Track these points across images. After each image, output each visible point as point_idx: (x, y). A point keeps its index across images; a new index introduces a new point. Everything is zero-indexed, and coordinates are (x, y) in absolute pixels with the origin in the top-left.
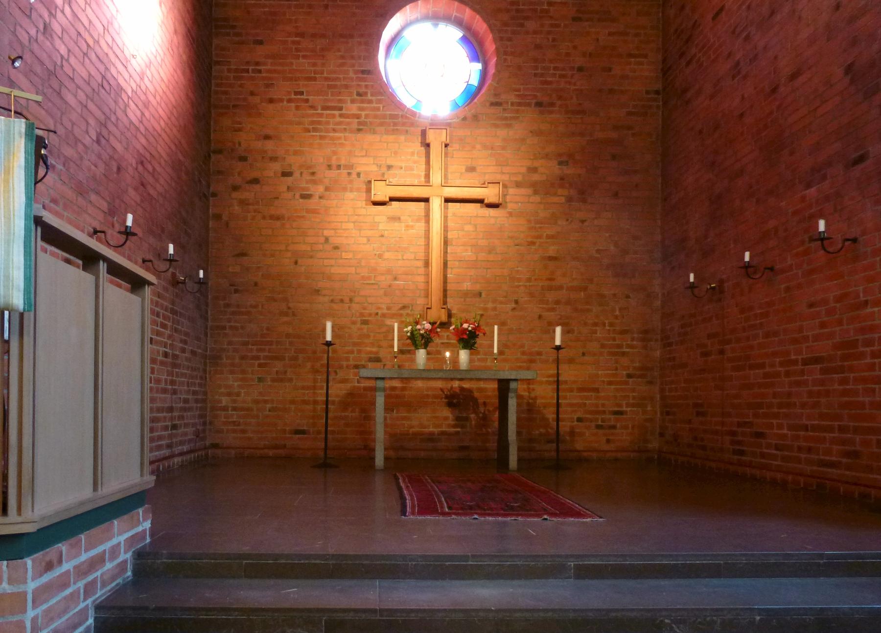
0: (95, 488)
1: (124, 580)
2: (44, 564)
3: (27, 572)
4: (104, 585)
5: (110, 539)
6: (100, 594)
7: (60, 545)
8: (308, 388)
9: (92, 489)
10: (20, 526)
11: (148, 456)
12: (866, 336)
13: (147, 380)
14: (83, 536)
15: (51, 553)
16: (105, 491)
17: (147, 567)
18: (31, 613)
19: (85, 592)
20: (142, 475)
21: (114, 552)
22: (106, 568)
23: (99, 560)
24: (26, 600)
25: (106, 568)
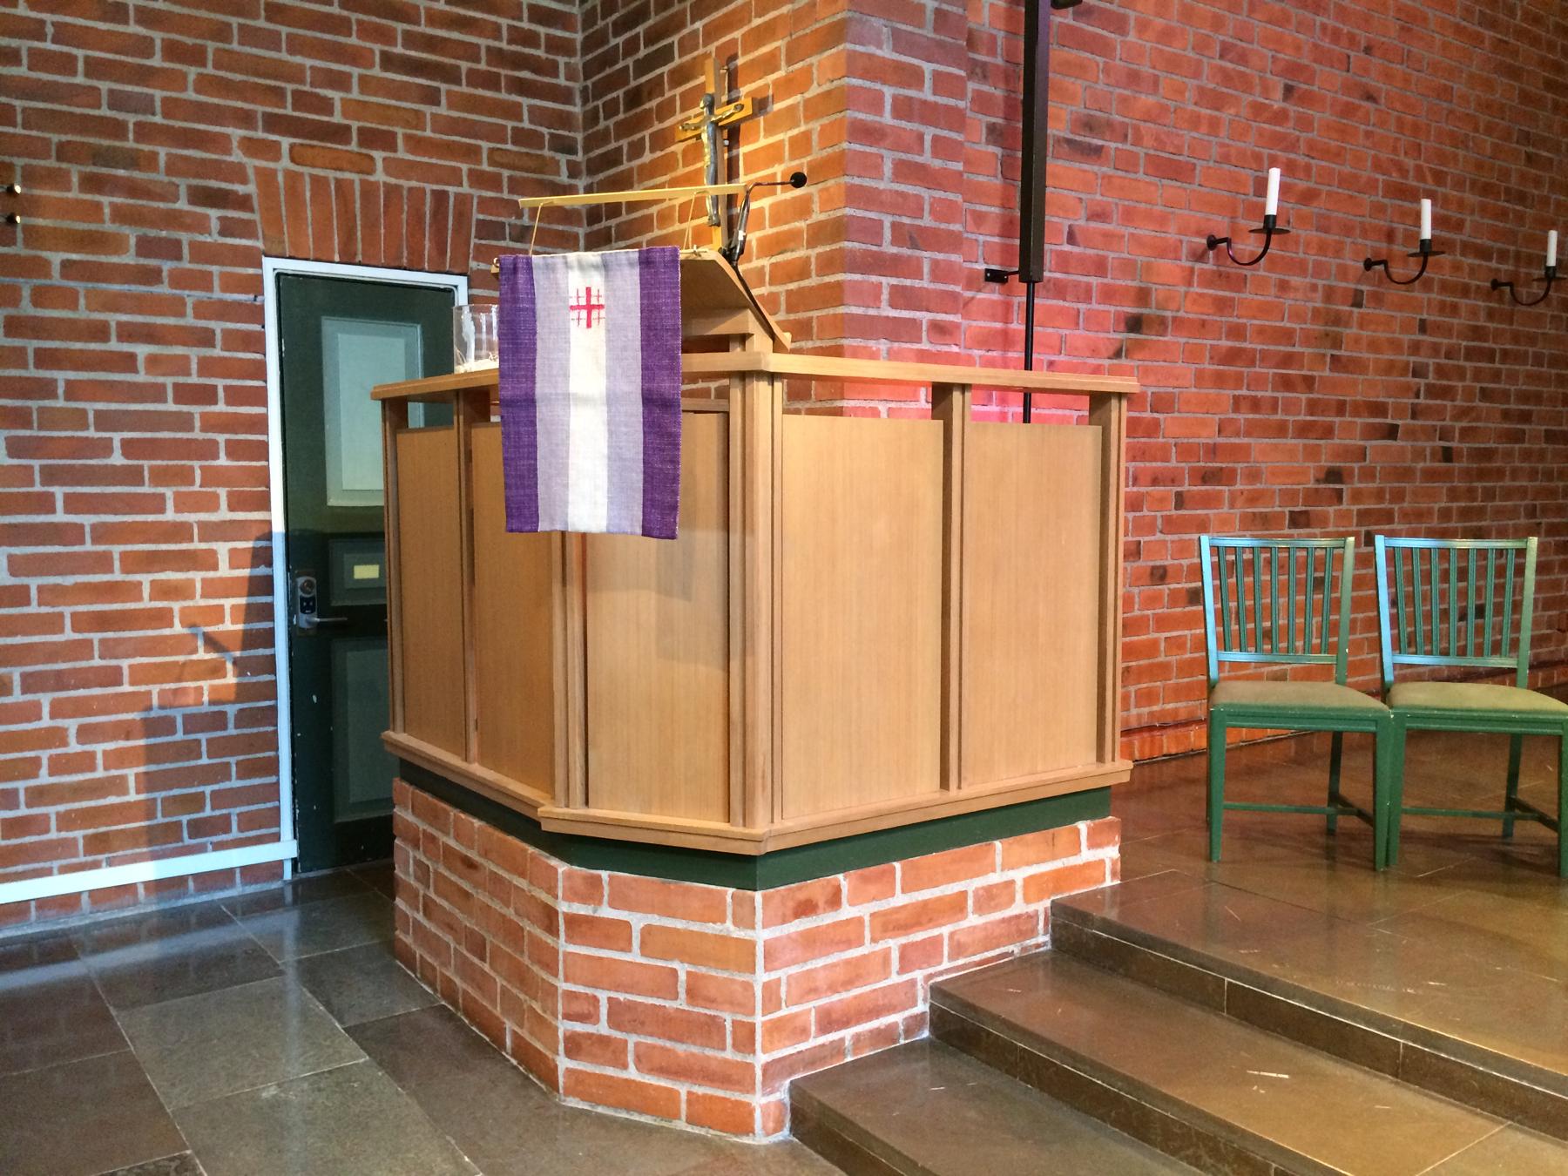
0: (944, 783)
1: (1024, 949)
2: (791, 904)
3: (754, 913)
4: (958, 950)
5: (985, 873)
6: (946, 967)
7: (841, 876)
8: (588, 300)
9: (1093, 756)
10: (738, 843)
11: (1116, 718)
12: (1155, 708)
13: (1118, 587)
14: (998, 844)
15: (815, 888)
16: (966, 791)
17: (1086, 945)
18: (761, 977)
19: (902, 958)
20: (1100, 758)
21: (990, 898)
22: (964, 924)
23: (956, 906)
24: (754, 955)
25: (964, 924)
